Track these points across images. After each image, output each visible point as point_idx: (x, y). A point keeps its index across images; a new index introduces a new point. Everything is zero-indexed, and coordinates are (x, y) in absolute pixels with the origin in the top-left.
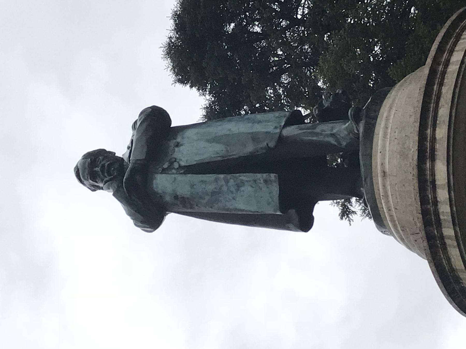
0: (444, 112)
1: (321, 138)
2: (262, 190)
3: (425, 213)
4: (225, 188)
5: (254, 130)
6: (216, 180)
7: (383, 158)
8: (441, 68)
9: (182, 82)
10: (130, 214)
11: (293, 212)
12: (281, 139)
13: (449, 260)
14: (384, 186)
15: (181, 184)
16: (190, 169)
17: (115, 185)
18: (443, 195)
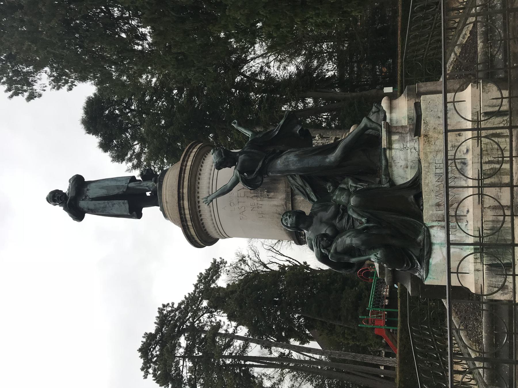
0: (186, 183)
1: (143, 187)
2: (124, 206)
3: (181, 218)
4: (108, 206)
5: (118, 184)
6: (104, 203)
9: (88, 133)
10: (70, 216)
11: (134, 213)
12: (128, 188)
13: (190, 232)
15: (92, 205)
18: (187, 212)
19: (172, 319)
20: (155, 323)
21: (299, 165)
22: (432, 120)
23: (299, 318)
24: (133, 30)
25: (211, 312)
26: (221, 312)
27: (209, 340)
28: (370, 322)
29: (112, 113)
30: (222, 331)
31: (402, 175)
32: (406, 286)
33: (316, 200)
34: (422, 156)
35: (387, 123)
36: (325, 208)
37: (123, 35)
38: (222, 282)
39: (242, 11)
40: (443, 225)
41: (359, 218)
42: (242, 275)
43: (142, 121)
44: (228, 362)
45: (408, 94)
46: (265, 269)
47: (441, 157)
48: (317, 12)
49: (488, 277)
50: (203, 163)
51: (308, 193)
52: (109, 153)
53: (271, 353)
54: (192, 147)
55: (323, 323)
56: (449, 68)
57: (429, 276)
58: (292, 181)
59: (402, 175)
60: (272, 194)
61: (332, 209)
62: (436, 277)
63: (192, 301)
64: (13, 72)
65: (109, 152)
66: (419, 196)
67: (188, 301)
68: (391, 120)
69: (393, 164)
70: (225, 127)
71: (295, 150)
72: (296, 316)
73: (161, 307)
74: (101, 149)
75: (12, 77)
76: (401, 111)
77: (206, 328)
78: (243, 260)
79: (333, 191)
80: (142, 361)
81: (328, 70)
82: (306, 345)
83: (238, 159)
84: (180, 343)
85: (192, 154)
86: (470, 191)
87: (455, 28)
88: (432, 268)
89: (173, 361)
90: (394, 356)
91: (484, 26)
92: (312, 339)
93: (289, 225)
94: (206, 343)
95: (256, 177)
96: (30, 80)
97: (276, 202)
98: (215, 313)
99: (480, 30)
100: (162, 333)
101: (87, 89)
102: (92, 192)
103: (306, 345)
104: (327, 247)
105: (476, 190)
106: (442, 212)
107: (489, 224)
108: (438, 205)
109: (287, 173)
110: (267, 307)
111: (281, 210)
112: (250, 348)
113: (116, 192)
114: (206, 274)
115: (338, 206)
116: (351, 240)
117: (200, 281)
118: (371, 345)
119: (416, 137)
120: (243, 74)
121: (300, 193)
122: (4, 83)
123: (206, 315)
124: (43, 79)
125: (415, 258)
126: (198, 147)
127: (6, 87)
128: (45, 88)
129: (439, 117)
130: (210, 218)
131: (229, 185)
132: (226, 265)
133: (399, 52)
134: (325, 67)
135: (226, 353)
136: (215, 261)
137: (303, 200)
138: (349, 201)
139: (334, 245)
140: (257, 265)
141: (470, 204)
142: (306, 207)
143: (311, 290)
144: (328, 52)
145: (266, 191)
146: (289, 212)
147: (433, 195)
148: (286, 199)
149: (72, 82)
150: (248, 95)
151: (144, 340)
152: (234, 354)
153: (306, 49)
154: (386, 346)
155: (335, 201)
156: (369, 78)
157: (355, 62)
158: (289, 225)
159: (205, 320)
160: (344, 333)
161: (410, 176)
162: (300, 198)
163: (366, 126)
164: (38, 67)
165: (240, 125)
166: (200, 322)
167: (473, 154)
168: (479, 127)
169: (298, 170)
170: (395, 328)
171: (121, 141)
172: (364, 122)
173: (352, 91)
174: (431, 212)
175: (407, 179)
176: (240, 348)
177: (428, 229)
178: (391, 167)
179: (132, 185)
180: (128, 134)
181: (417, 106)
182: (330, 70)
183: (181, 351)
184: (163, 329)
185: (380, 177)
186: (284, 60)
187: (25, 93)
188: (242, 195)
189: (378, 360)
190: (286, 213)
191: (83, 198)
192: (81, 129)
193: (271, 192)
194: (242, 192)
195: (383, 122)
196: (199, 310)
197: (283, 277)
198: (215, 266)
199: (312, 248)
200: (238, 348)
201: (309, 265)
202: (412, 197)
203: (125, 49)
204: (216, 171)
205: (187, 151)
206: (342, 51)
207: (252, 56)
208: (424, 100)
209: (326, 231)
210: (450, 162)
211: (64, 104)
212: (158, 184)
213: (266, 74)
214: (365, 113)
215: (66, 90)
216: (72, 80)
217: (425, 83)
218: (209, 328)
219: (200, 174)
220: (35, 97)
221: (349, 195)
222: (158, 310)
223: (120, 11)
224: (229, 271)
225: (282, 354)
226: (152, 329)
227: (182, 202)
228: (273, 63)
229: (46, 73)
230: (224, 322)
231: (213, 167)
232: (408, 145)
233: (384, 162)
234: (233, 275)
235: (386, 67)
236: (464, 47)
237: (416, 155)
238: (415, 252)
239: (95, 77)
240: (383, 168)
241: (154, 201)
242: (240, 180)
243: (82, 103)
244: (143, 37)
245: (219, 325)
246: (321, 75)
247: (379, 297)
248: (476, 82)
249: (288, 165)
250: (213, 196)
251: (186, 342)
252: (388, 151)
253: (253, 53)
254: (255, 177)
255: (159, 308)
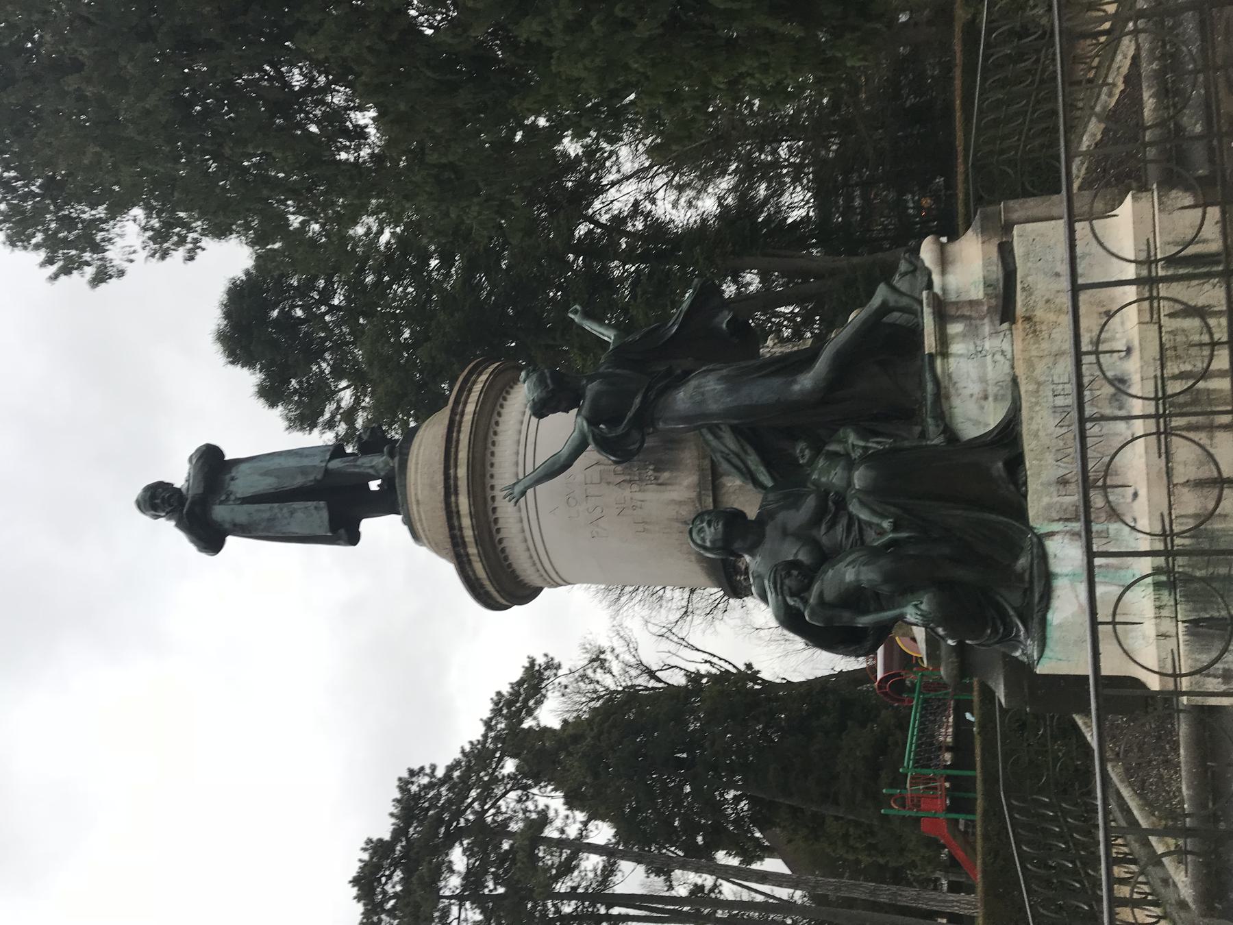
0: (463, 455)
1: (362, 470)
2: (316, 514)
3: (453, 537)
4: (279, 515)
6: (271, 509)
7: (416, 489)
8: (458, 418)
9: (232, 363)
10: (192, 541)
11: (342, 531)
13: (474, 572)
14: (418, 512)
15: (242, 513)
16: (246, 500)
17: (177, 515)
18: (466, 522)
19: (431, 804)
20: (392, 815)
21: (729, 401)
22: (1041, 283)
23: (737, 800)
24: (335, 117)
25: (525, 788)
26: (550, 788)
27: (520, 855)
28: (908, 803)
29: (286, 315)
30: (551, 832)
31: (975, 416)
32: (991, 684)
33: (770, 484)
34: (1020, 371)
35: (935, 295)
36: (794, 502)
37: (314, 129)
38: (550, 714)
39: (587, 61)
40: (1077, 529)
41: (875, 520)
42: (599, 698)
43: (357, 332)
44: (567, 909)
45: (982, 227)
46: (652, 684)
47: (1065, 366)
48: (765, 60)
49: (1191, 651)
50: (502, 406)
51: (753, 468)
52: (280, 409)
53: (671, 887)
54: (477, 371)
55: (795, 811)
56: (1079, 170)
57: (1047, 652)
58: (714, 443)
59: (975, 416)
60: (666, 475)
61: (810, 502)
62: (1063, 656)
63: (478, 758)
64: (58, 219)
65: (280, 408)
66: (1016, 463)
67: (470, 761)
68: (944, 290)
69: (952, 391)
70: (551, 342)
71: (718, 366)
72: (730, 795)
73: (405, 775)
74: (262, 400)
75: (56, 232)
76: (967, 266)
77: (514, 827)
78: (598, 660)
79: (812, 462)
80: (359, 908)
81: (791, 207)
82: (756, 866)
83: (584, 393)
84: (450, 862)
85: (478, 387)
86: (1139, 427)
87: (1090, 81)
88: (1053, 634)
89: (435, 908)
90: (970, 889)
91: (1158, 59)
92: (770, 852)
93: (708, 544)
94: (513, 862)
95: (627, 435)
96: (98, 238)
97: (677, 492)
98: (535, 791)
99: (1148, 68)
100: (408, 840)
101: (231, 258)
102: (242, 484)
103: (756, 866)
104: (801, 592)
105: (1151, 425)
106: (1073, 498)
107: (1187, 524)
108: (1063, 482)
109: (699, 421)
110: (661, 775)
111: (687, 512)
112: (619, 874)
113: (299, 481)
114: (511, 694)
115: (824, 494)
116: (858, 574)
117: (497, 712)
118: (913, 865)
119: (1006, 325)
120: (591, 219)
121: (733, 470)
122: (37, 247)
123: (513, 795)
124: (129, 233)
125: (1012, 613)
126: (490, 369)
127: (42, 255)
128: (132, 257)
129: (1057, 275)
130: (520, 536)
131: (565, 452)
132: (560, 672)
133: (960, 149)
134: (786, 199)
135: (562, 887)
136: (532, 662)
137: (740, 487)
138: (850, 483)
139: (816, 589)
140: (634, 672)
141: (1137, 463)
142: (746, 500)
143: (764, 733)
144: (790, 165)
145: (651, 467)
146: (709, 512)
147: (1050, 458)
148: (700, 485)
149: (196, 241)
150: (605, 268)
151: (366, 856)
152: (580, 890)
153: (739, 159)
154: (953, 864)
155: (816, 484)
156: (890, 224)
157: (857, 185)
158: (708, 544)
159: (512, 805)
160: (846, 836)
161: (993, 417)
162: (733, 483)
163: (884, 303)
164: (118, 208)
165: (587, 315)
166: (499, 812)
167: (1141, 358)
168: (1154, 274)
169: (727, 414)
170: (970, 817)
171: (308, 382)
172: (881, 294)
173: (852, 253)
174: (1046, 500)
175: (987, 425)
176: (596, 875)
177: (1040, 539)
178: (948, 398)
179: (336, 464)
180: (324, 365)
181: (1006, 251)
182: (797, 204)
183: (453, 883)
184: (411, 830)
185: (922, 422)
186: (688, 185)
187: (86, 268)
188: (596, 479)
189: (933, 900)
190: (699, 516)
191: (223, 498)
192: (215, 354)
193: (664, 470)
194: (595, 473)
195: (925, 293)
196: (495, 780)
197: (696, 701)
198: (533, 676)
199: (764, 598)
200: (591, 875)
201: (758, 672)
202: (1000, 464)
203: (316, 157)
204: (534, 420)
205: (466, 381)
206: (825, 161)
207: (613, 177)
208: (1021, 237)
209: (796, 554)
210: (1087, 359)
211: (174, 292)
212: (397, 459)
213: (645, 220)
214: (887, 273)
215: (181, 259)
216: (195, 235)
217: (1021, 201)
218: (521, 825)
219: (495, 433)
220: (111, 277)
221: (851, 465)
222: (397, 783)
223: (305, 76)
224: (566, 687)
225: (698, 889)
226: (384, 830)
227: (453, 499)
228: (661, 192)
229: (135, 220)
230: (556, 811)
231: (528, 412)
232: (987, 345)
233: (930, 387)
234: (577, 698)
235: (931, 197)
236: (1111, 117)
237: (1007, 369)
238: (1010, 600)
239: (247, 227)
240: (929, 402)
241: (388, 502)
242: (590, 440)
243: (217, 293)
244: (359, 133)
245: (544, 818)
246: (776, 222)
247: (928, 751)
248: (1144, 188)
249: (703, 402)
250: (527, 482)
251: (465, 859)
252: (939, 362)
253: (614, 169)
254: (625, 434)
255: (400, 779)
